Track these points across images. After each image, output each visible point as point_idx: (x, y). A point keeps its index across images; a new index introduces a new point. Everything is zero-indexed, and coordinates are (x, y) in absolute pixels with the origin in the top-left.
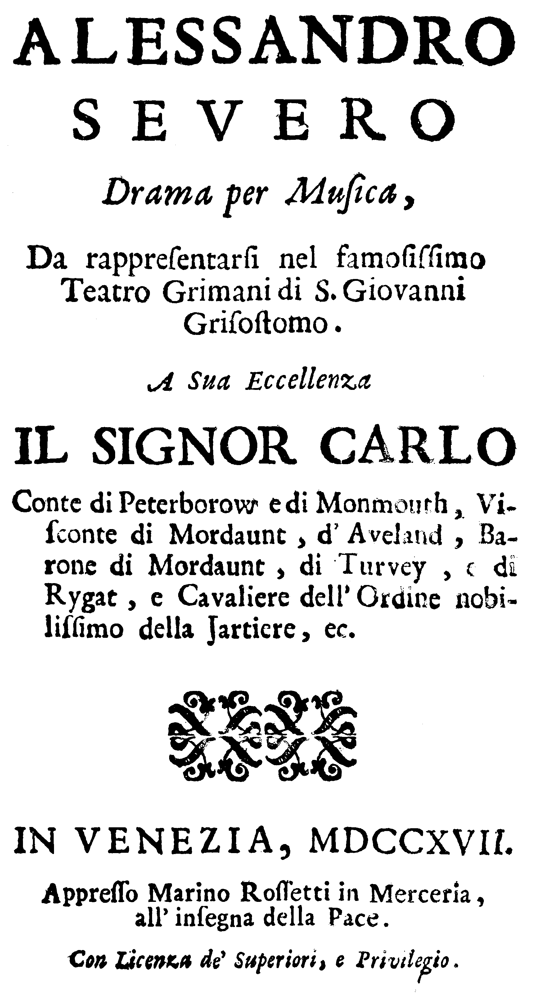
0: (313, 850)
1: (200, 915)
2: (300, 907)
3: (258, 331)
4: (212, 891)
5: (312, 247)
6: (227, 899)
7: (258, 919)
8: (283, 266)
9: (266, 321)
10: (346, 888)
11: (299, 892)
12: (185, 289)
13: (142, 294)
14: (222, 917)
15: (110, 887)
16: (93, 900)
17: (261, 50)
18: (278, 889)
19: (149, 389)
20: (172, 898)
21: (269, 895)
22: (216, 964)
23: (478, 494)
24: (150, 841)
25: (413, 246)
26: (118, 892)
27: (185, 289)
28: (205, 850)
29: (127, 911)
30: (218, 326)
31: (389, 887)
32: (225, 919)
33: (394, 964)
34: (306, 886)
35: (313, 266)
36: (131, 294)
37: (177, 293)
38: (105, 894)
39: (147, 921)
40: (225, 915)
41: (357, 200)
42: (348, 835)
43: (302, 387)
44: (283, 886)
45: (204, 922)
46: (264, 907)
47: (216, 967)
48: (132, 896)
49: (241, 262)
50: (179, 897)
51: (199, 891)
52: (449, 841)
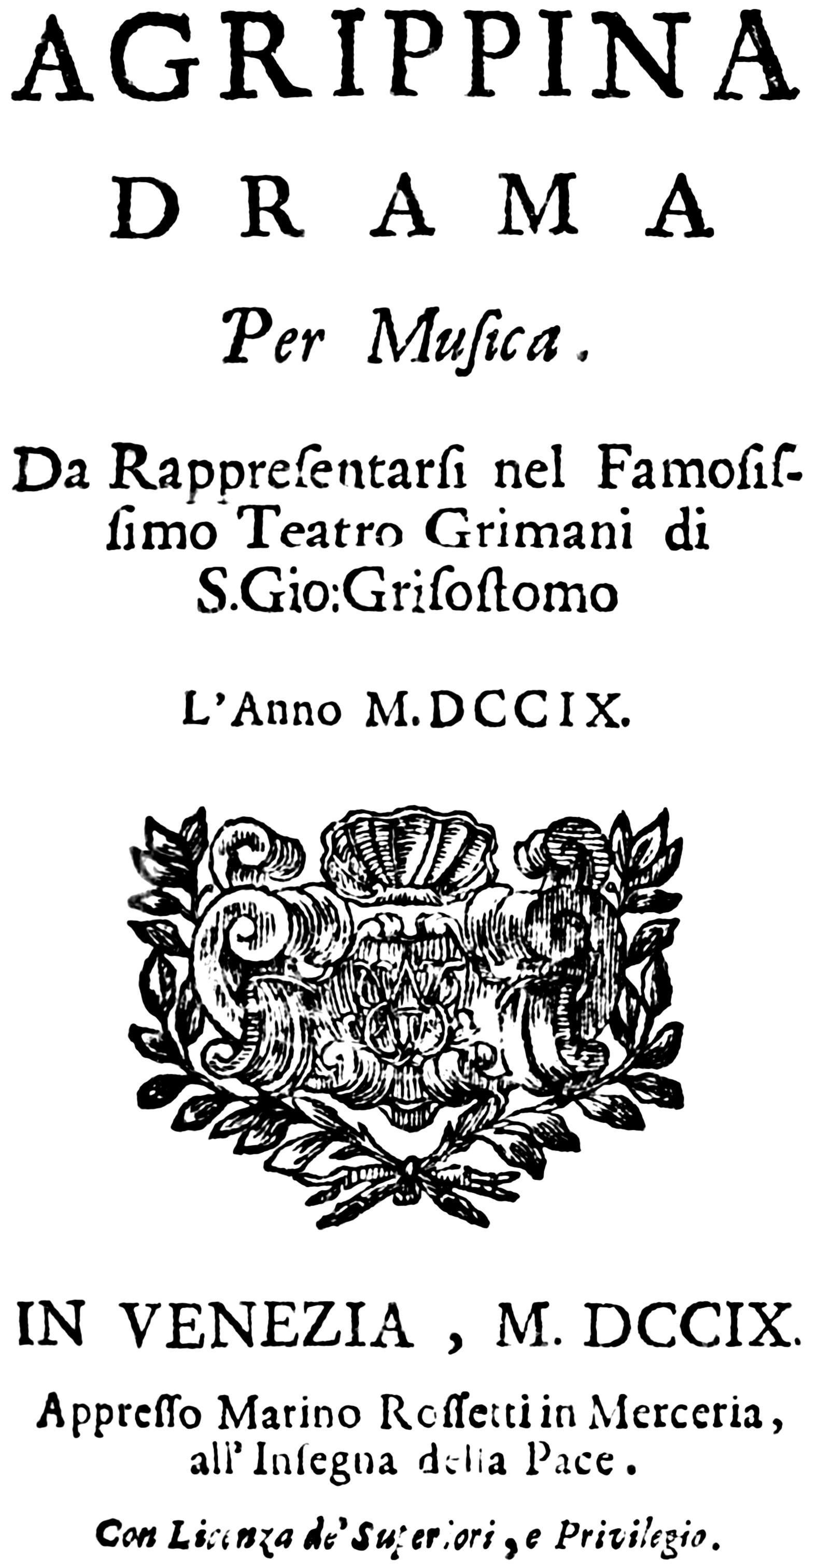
3: (483, 608)
5: (557, 449)
8: (500, 484)
9: (499, 587)
12: (283, 586)
18: (482, 587)
22: (329, 1541)
25: (758, 447)
26: (168, 1409)
27: (283, 586)
28: (328, 1306)
29: (181, 1443)
32: (345, 1461)
33: (618, 1540)
35: (558, 483)
37: (414, 93)
39: (210, 1464)
40: (345, 1455)
41: (490, 355)
44: (492, 578)
46: (417, 1441)
47: (328, 1546)
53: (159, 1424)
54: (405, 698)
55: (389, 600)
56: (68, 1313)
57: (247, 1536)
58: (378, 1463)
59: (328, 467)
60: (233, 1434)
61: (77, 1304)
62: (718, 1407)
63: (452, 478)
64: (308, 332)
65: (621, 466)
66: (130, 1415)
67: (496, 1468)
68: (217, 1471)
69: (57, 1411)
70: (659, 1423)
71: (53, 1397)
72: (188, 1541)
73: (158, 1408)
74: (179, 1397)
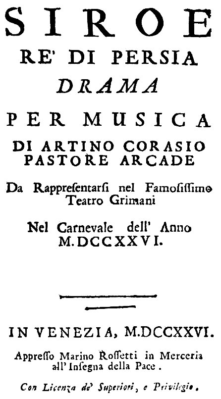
0: (127, 335)
1: (80, 366)
2: (124, 362)
5: (133, 184)
6: (92, 358)
7: (105, 367)
10: (148, 354)
12: (119, 199)
13: (100, 202)
18: (115, 354)
21: (111, 357)
23: (116, 237)
24: (65, 332)
25: (182, 183)
26: (47, 356)
27: (119, 199)
28: (85, 336)
30: (124, 201)
31: (68, 354)
35: (133, 191)
36: (95, 201)
42: (143, 329)
44: (116, 353)
45: (82, 368)
49: (101, 189)
50: (73, 358)
52: (193, 332)
54: (100, 115)
55: (120, 202)
57: (64, 388)
58: (99, 367)
59: (79, 187)
60: (64, 361)
61: (26, 328)
63: (105, 189)
65: (151, 187)
69: (20, 356)
73: (44, 355)
74: (49, 352)
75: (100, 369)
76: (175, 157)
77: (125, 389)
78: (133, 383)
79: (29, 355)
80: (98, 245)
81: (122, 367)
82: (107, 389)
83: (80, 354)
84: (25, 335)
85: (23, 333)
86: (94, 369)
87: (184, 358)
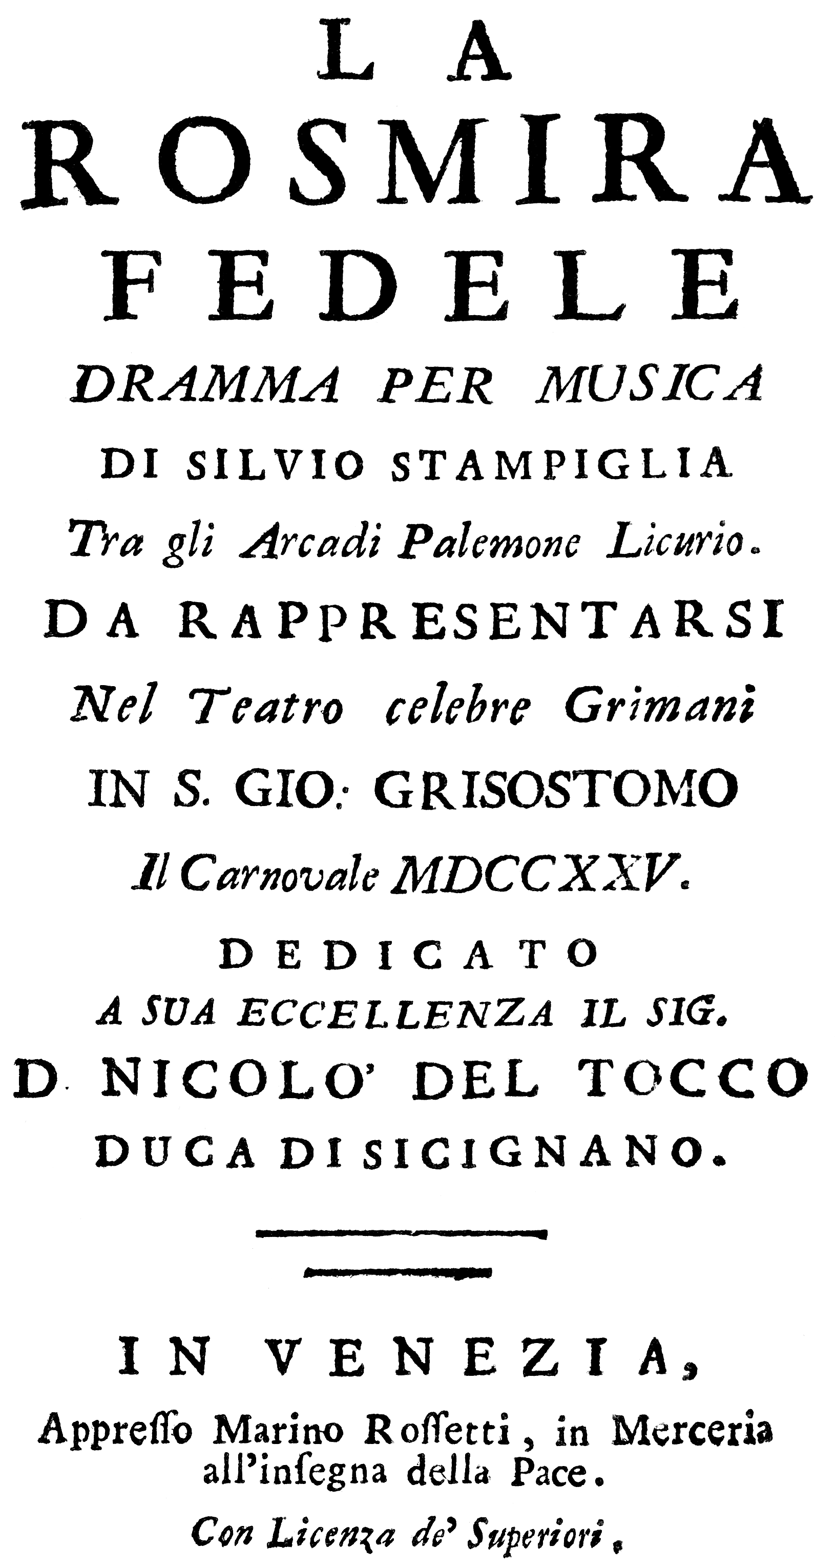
1: (299, 1466)
4: (316, 1427)
11: (459, 1429)
14: (337, 1470)
15: (147, 1422)
16: (118, 1440)
17: (462, 66)
18: (425, 1425)
19: (717, 369)
20: (251, 1437)
26: (167, 1429)
32: (341, 1473)
34: (488, 1423)
38: (137, 1430)
39: (221, 1474)
40: (342, 1466)
43: (435, 718)
48: (183, 1432)
51: (295, 1427)
53: (155, 1441)
56: (555, 1145)
57: (350, 1535)
61: (202, 1341)
62: (734, 1427)
64: (450, 555)
66: (125, 1434)
67: (211, 1478)
68: (226, 1480)
70: (733, 1442)
71: (54, 1416)
72: (292, 1539)
75: (375, 1480)
76: (348, 260)
77: (568, 1544)
78: (600, 1522)
79: (96, 1424)
80: (209, 1161)
81: (460, 1476)
82: (500, 1543)
83: (290, 1422)
84: (200, 1367)
85: (190, 1357)
86: (354, 1481)
87: (564, 1484)
